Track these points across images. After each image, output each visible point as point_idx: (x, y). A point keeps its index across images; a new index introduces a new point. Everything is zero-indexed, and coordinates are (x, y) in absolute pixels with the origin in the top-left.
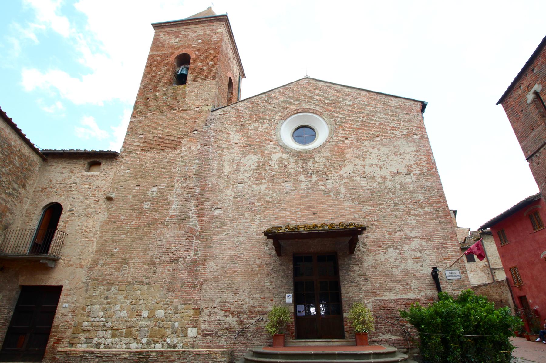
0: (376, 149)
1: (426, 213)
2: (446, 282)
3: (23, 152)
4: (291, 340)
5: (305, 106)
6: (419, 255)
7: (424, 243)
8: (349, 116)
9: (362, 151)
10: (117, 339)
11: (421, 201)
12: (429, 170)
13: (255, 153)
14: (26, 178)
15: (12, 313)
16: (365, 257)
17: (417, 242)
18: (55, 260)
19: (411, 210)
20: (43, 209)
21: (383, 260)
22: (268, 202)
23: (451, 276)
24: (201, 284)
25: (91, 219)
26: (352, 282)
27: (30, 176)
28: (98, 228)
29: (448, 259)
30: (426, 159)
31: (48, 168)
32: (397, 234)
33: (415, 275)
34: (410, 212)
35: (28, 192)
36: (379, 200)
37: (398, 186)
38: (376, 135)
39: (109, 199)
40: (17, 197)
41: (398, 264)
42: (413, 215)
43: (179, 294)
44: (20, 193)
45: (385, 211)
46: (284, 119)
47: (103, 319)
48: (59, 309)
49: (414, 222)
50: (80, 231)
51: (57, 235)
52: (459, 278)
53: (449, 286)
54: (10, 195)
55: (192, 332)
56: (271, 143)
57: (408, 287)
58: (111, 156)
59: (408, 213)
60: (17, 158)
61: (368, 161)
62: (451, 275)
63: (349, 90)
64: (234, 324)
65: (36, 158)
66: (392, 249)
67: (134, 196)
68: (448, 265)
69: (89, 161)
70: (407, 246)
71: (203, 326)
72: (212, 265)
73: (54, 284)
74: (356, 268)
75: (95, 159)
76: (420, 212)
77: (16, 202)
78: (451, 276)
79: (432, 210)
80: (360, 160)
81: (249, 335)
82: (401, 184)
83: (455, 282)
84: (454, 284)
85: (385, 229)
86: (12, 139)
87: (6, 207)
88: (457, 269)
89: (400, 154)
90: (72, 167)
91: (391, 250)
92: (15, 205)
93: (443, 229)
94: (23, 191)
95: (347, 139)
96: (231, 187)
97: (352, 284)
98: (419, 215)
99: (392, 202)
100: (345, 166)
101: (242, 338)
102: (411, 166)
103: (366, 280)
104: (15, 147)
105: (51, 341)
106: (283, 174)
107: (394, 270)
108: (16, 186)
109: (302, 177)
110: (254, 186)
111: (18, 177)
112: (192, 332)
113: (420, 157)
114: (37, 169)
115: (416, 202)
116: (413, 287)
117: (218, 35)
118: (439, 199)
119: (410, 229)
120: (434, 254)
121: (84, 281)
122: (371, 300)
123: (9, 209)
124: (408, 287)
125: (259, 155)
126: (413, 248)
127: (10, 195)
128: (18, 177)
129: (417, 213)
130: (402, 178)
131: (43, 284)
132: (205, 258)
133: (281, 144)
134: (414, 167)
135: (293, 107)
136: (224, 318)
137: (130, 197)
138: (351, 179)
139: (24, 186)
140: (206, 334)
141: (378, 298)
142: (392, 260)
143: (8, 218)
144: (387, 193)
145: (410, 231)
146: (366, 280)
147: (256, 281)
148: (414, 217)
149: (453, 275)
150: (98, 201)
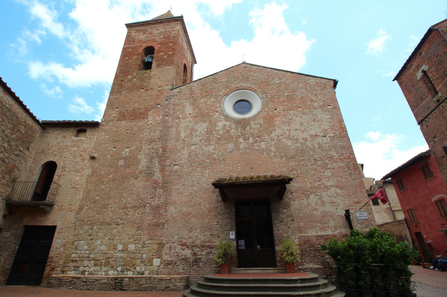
0: (299, 117)
1: (340, 167)
2: (357, 222)
3: (28, 122)
4: (234, 269)
5: (243, 85)
6: (334, 200)
7: (338, 191)
8: (277, 92)
9: (287, 119)
10: (98, 268)
11: (335, 157)
12: (340, 133)
13: (205, 122)
14: (30, 142)
15: (17, 247)
16: (292, 202)
17: (333, 190)
18: (51, 206)
19: (327, 164)
20: (42, 166)
21: (306, 204)
22: (215, 160)
23: (361, 217)
24: (163, 224)
25: (79, 174)
26: (282, 222)
27: (32, 141)
28: (84, 181)
29: (358, 203)
30: (338, 124)
31: (46, 134)
32: (317, 184)
33: (332, 216)
34: (326, 166)
35: (31, 153)
36: (302, 157)
37: (317, 146)
38: (299, 106)
39: (93, 158)
40: (23, 157)
41: (318, 207)
42: (329, 169)
43: (146, 232)
44: (25, 154)
45: (307, 166)
46: (227, 95)
47: (88, 252)
48: (53, 244)
49: (330, 174)
50: (70, 183)
51: (53, 186)
52: (367, 218)
53: (359, 225)
54: (17, 155)
55: (156, 262)
56: (217, 113)
57: (327, 226)
58: (94, 125)
59: (325, 167)
60: (23, 127)
61: (293, 127)
62: (360, 216)
63: (277, 72)
64: (189, 255)
65: (37, 127)
66: (313, 195)
67: (112, 156)
68: (358, 208)
69: (77, 129)
70: (325, 193)
71: (165, 257)
72: (171, 209)
73: (50, 224)
74: (285, 211)
75: (82, 127)
76: (335, 166)
77: (22, 161)
78: (361, 217)
79: (344, 165)
80: (286, 125)
81: (201, 264)
82: (319, 144)
83: (363, 222)
84: (363, 223)
85: (307, 179)
86: (19, 113)
87: (14, 165)
88: (365, 211)
89: (318, 121)
90: (65, 134)
91: (312, 196)
92: (21, 163)
93: (353, 179)
94: (27, 153)
95: (276, 109)
96: (186, 148)
97: (282, 224)
98: (334, 169)
99: (312, 159)
100: (275, 130)
101: (196, 267)
102: (327, 130)
103: (293, 220)
104: (22, 119)
105: (47, 269)
106: (226, 137)
107: (315, 212)
108: (22, 148)
109: (241, 140)
110: (204, 147)
111: (23, 142)
112: (156, 262)
113: (334, 123)
114: (38, 135)
115: (331, 158)
116: (330, 225)
117: (176, 32)
118: (349, 156)
119: (327, 179)
120: (347, 200)
121: (73, 222)
122: (297, 237)
123: (16, 167)
124: (327, 226)
125: (208, 123)
126: (330, 195)
127: (17, 155)
128: (23, 142)
129: (332, 167)
130: (319, 140)
131: (41, 224)
132: (166, 204)
133: (224, 114)
134: (329, 130)
135: (234, 86)
136: (181, 251)
137: (109, 156)
138: (279, 141)
139: (28, 149)
140: (167, 264)
141: (303, 234)
142: (313, 204)
143: (16, 174)
144: (308, 151)
145: (327, 181)
146: (293, 220)
147: (206, 221)
148: (330, 170)
149: (362, 216)
150: (84, 160)
